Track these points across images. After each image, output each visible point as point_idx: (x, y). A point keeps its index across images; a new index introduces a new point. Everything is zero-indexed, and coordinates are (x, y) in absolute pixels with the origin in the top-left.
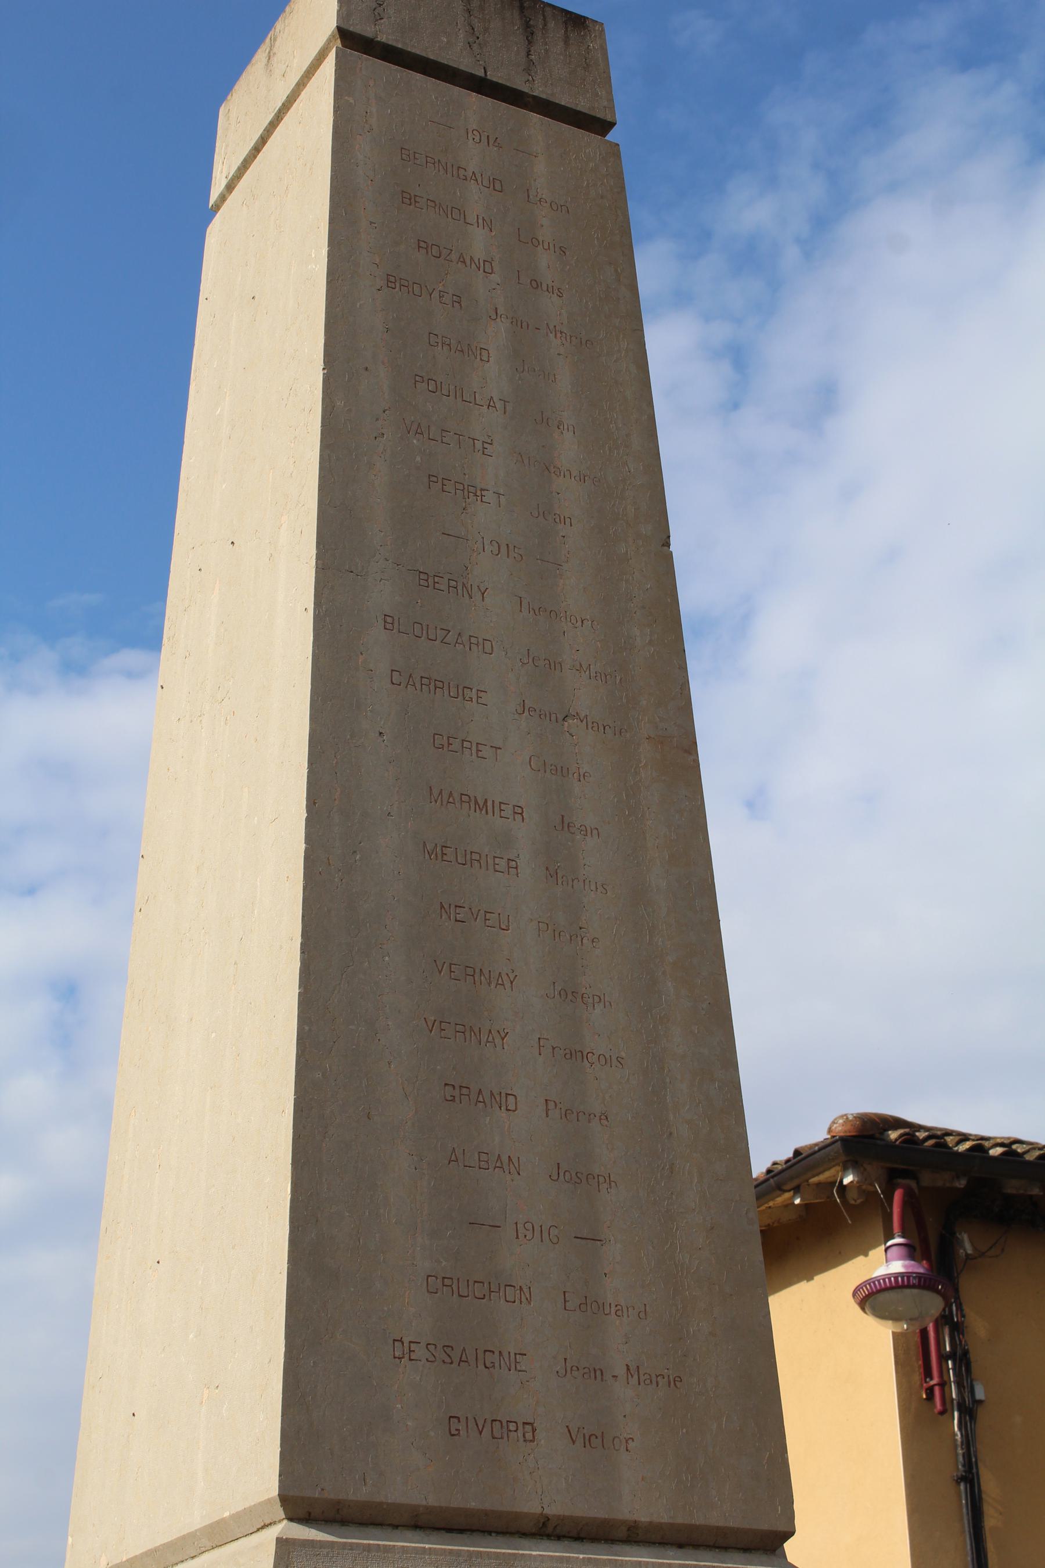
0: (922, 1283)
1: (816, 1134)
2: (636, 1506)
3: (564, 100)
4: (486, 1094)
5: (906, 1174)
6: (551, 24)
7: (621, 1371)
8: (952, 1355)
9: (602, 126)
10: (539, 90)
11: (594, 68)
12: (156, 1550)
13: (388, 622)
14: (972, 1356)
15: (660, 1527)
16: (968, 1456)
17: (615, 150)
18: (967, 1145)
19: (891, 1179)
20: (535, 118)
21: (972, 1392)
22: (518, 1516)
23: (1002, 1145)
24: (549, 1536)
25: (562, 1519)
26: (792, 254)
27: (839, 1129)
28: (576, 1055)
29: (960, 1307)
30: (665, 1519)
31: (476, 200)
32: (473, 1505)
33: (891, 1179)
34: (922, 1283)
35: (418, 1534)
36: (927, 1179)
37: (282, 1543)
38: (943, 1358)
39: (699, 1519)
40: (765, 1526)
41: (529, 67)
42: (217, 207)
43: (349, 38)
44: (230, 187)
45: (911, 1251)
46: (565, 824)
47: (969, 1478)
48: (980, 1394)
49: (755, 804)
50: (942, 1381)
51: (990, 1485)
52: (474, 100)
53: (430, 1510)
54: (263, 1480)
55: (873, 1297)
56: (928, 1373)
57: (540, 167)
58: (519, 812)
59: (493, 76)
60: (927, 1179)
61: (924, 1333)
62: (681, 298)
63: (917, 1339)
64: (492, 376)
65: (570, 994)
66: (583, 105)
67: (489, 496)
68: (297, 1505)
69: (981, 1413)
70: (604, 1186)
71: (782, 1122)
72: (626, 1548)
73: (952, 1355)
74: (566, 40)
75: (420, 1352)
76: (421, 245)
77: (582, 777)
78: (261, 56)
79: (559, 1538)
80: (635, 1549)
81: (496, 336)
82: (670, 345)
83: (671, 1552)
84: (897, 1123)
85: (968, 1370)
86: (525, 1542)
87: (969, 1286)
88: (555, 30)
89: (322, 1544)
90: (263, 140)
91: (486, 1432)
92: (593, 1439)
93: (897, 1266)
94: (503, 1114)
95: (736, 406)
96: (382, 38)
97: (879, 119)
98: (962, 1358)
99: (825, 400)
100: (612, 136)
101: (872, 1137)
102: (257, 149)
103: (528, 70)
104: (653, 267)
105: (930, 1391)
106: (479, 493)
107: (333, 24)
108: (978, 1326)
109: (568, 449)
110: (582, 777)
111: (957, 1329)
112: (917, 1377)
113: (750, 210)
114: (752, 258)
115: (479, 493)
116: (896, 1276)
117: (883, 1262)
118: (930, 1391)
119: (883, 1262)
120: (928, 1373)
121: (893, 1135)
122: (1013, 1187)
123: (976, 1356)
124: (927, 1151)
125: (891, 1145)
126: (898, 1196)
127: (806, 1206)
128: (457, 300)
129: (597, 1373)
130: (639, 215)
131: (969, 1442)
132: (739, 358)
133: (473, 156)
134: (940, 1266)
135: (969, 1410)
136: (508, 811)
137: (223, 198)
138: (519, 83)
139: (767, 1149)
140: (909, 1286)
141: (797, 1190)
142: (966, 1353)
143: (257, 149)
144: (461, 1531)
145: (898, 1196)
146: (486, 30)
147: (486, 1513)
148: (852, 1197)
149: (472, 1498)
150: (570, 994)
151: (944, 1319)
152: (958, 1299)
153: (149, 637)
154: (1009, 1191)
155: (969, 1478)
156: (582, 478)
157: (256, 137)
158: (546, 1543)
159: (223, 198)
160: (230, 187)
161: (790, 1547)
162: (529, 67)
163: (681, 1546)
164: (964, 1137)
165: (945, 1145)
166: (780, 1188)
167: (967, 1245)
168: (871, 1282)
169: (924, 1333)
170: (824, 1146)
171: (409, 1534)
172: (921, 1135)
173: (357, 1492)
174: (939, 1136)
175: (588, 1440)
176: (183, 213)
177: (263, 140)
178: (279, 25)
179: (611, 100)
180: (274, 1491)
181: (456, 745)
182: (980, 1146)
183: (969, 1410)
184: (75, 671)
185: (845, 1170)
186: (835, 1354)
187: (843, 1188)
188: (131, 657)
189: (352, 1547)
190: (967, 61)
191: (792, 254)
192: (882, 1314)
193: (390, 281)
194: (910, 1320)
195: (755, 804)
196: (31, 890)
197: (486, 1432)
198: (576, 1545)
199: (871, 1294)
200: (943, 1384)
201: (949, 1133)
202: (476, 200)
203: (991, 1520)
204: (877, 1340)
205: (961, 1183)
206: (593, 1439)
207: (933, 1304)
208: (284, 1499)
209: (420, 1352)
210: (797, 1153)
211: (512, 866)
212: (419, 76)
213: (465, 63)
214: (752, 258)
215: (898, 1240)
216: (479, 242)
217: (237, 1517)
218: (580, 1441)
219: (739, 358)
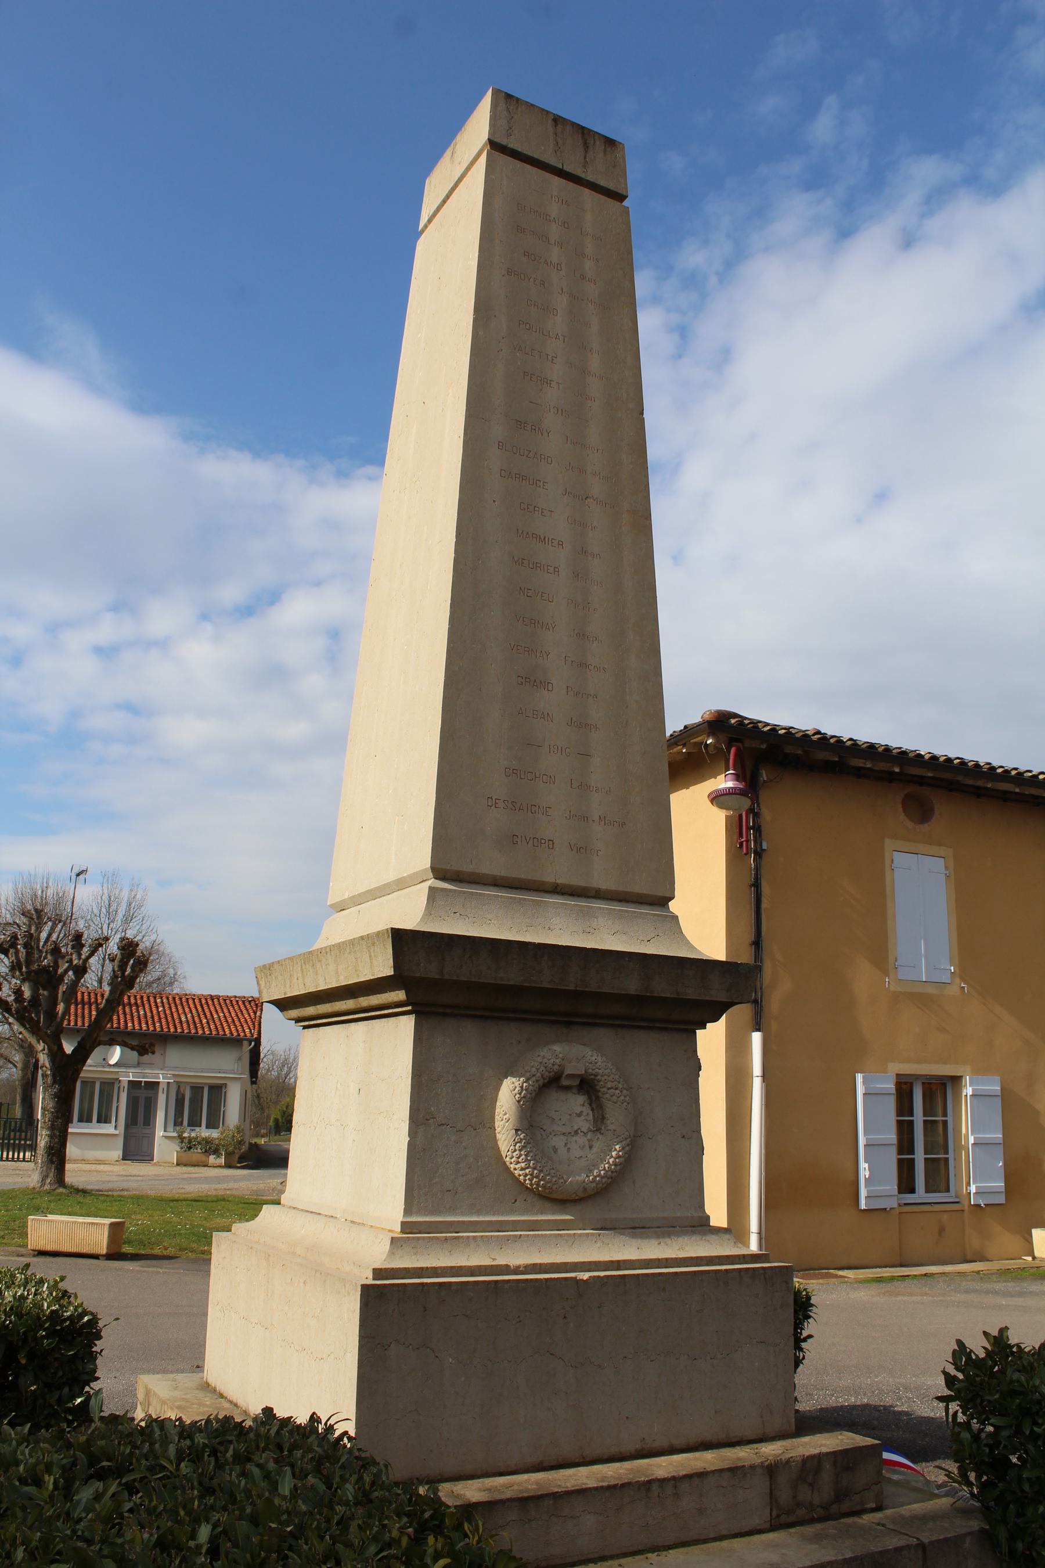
0: (742, 793)
1: (696, 719)
2: (601, 881)
3: (602, 183)
4: (538, 682)
5: (737, 740)
6: (598, 143)
7: (596, 818)
8: (753, 828)
9: (621, 197)
10: (590, 177)
11: (618, 168)
12: (371, 890)
13: (500, 445)
14: (763, 829)
15: (611, 891)
16: (756, 875)
17: (626, 210)
18: (768, 728)
19: (731, 742)
20: (587, 191)
21: (761, 845)
22: (543, 883)
23: (785, 729)
24: (558, 893)
25: (565, 885)
26: (713, 280)
27: (707, 717)
28: (583, 665)
29: (758, 805)
30: (613, 888)
31: (555, 231)
32: (523, 876)
33: (731, 742)
34: (742, 793)
35: (496, 889)
36: (748, 743)
37: (431, 889)
38: (748, 828)
39: (629, 889)
40: (660, 894)
41: (585, 165)
42: (423, 231)
43: (495, 146)
44: (430, 221)
45: (737, 777)
46: (584, 552)
47: (756, 885)
48: (765, 846)
49: (677, 558)
50: (747, 840)
51: (766, 889)
52: (556, 181)
53: (502, 878)
54: (424, 861)
55: (717, 798)
56: (741, 835)
57: (588, 216)
58: (561, 544)
59: (567, 168)
60: (748, 743)
61: (740, 816)
62: (656, 300)
63: (737, 819)
64: (558, 323)
65: (582, 636)
66: (611, 186)
67: (554, 384)
68: (439, 872)
69: (764, 855)
70: (593, 730)
71: (682, 710)
72: (594, 900)
73: (753, 828)
74: (605, 152)
75: (501, 804)
76: (526, 254)
77: (593, 528)
78: (448, 153)
79: (563, 894)
80: (599, 901)
81: (561, 303)
82: (650, 324)
83: (615, 903)
84: (735, 715)
85: (760, 835)
86: (546, 895)
87: (764, 795)
88: (599, 145)
89: (450, 890)
90: (448, 197)
91: (531, 842)
92: (582, 850)
93: (730, 784)
94: (546, 692)
95: (680, 357)
96: (511, 146)
97: (761, 213)
98: (758, 829)
99: (725, 356)
100: (626, 203)
101: (722, 721)
102: (444, 202)
103: (584, 166)
104: (643, 283)
105: (741, 844)
106: (549, 383)
107: (484, 136)
108: (766, 815)
109: (595, 363)
110: (593, 528)
111: (756, 815)
112: (735, 837)
113: (694, 257)
114: (693, 281)
115: (549, 383)
116: (729, 788)
117: (724, 782)
118: (741, 844)
119: (724, 782)
120: (741, 835)
121: (733, 721)
122: (789, 749)
123: (765, 829)
124: (749, 730)
125: (731, 726)
126: (733, 750)
127: (688, 753)
128: (543, 283)
129: (585, 819)
130: (638, 256)
131: (757, 868)
132: (683, 333)
133: (554, 210)
134: (750, 785)
135: (759, 854)
136: (556, 543)
137: (426, 226)
138: (579, 172)
139: (673, 725)
140: (735, 794)
141: (684, 745)
142: (760, 827)
143: (444, 202)
144: (516, 888)
145: (733, 750)
146: (564, 144)
147: (529, 881)
148: (711, 750)
149: (523, 874)
150: (582, 636)
151: (751, 811)
152: (758, 801)
153: (379, 459)
154: (786, 751)
155: (756, 885)
156: (601, 378)
157: (444, 195)
158: (557, 896)
159: (426, 226)
160: (430, 221)
161: (673, 905)
162: (585, 165)
163: (620, 901)
164: (767, 724)
165: (757, 727)
166: (676, 744)
167: (764, 776)
168: (717, 791)
169: (740, 816)
170: (699, 725)
171: (491, 888)
172: (746, 722)
173: (467, 868)
174: (755, 723)
175: (579, 850)
176: (404, 232)
177: (448, 197)
178: (458, 137)
179: (626, 184)
180: (427, 864)
181: (531, 508)
182: (774, 729)
183: (759, 854)
184: (343, 475)
185: (708, 736)
186: (699, 823)
187: (706, 745)
188: (370, 470)
189: (464, 892)
190: (809, 186)
191: (713, 280)
192: (721, 806)
193: (509, 272)
194: (734, 810)
195: (677, 558)
196: (318, 584)
197: (531, 842)
198: (571, 898)
199: (717, 797)
200: (748, 841)
201: (760, 722)
202: (555, 231)
203: (765, 905)
204: (718, 819)
205: (764, 746)
206: (582, 850)
207: (746, 803)
208: (433, 869)
209: (501, 804)
210: (686, 727)
211: (556, 570)
212: (528, 166)
213: (553, 161)
214: (693, 281)
215: (731, 772)
216: (555, 254)
217: (410, 876)
218: (575, 849)
219: (683, 333)
